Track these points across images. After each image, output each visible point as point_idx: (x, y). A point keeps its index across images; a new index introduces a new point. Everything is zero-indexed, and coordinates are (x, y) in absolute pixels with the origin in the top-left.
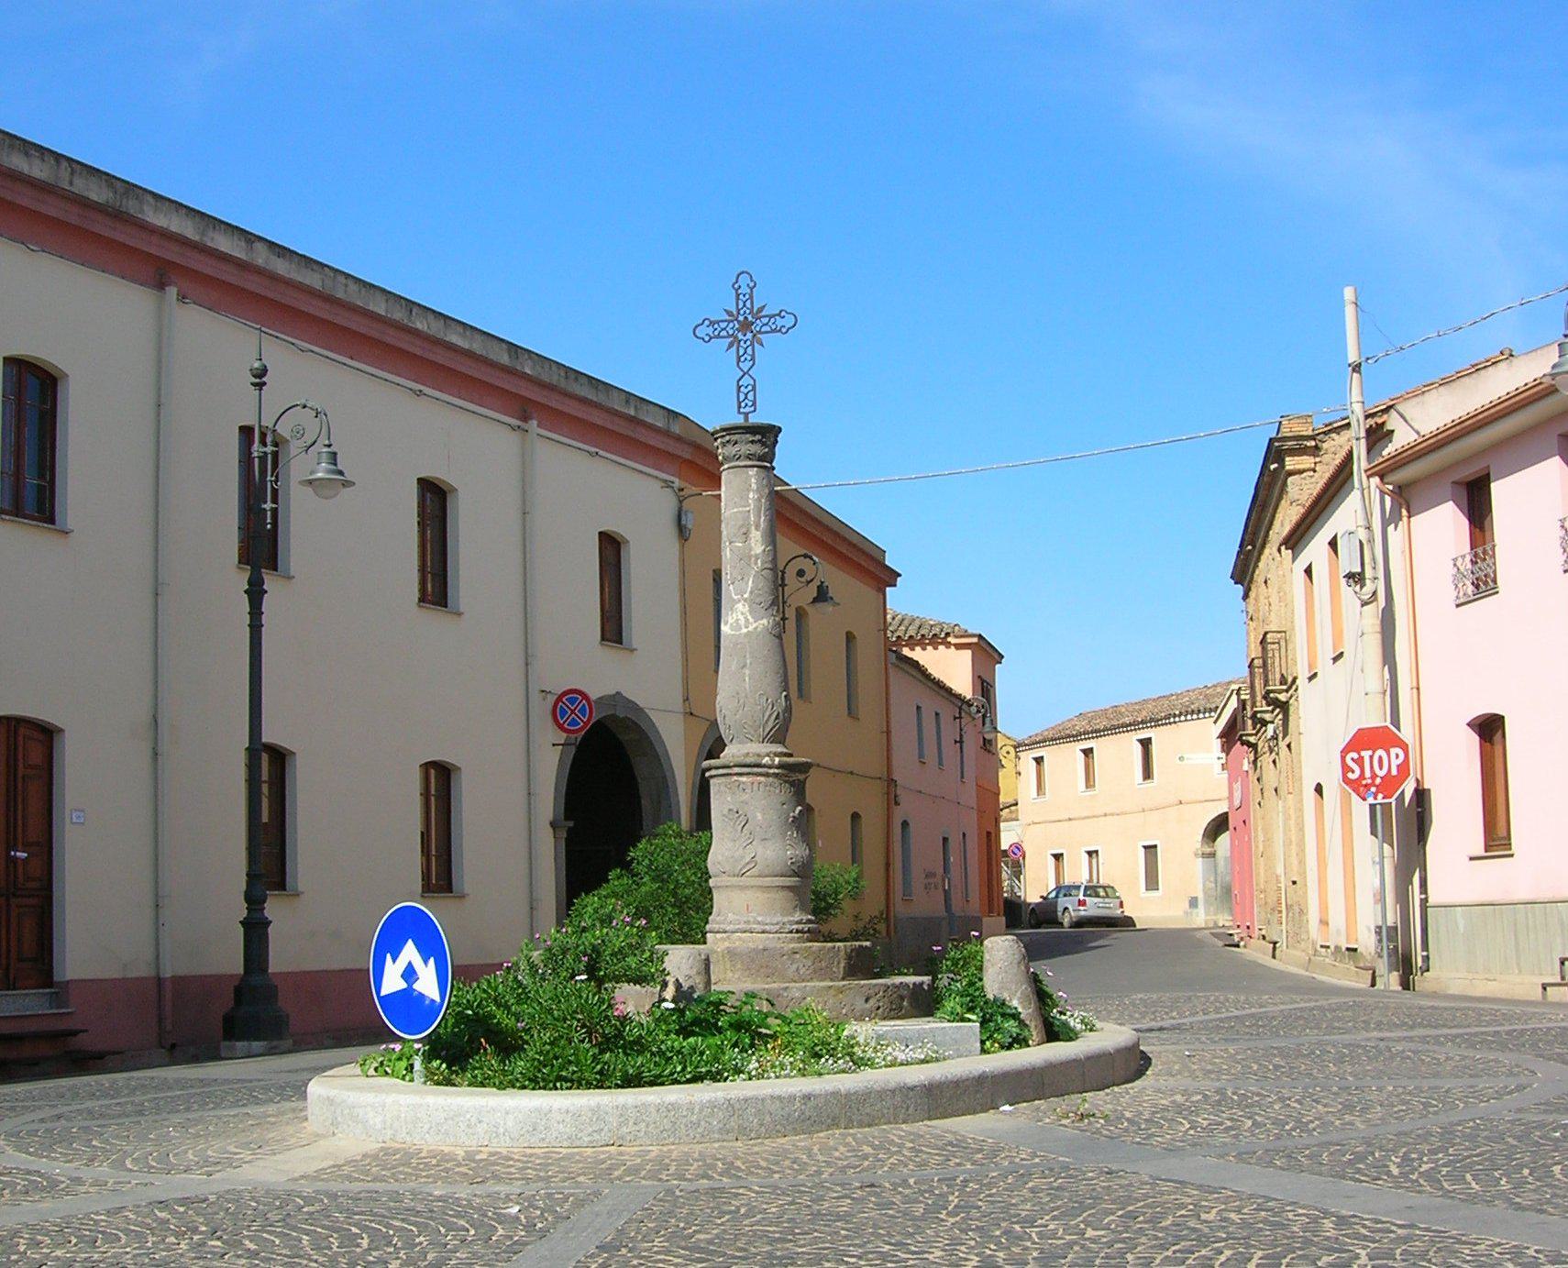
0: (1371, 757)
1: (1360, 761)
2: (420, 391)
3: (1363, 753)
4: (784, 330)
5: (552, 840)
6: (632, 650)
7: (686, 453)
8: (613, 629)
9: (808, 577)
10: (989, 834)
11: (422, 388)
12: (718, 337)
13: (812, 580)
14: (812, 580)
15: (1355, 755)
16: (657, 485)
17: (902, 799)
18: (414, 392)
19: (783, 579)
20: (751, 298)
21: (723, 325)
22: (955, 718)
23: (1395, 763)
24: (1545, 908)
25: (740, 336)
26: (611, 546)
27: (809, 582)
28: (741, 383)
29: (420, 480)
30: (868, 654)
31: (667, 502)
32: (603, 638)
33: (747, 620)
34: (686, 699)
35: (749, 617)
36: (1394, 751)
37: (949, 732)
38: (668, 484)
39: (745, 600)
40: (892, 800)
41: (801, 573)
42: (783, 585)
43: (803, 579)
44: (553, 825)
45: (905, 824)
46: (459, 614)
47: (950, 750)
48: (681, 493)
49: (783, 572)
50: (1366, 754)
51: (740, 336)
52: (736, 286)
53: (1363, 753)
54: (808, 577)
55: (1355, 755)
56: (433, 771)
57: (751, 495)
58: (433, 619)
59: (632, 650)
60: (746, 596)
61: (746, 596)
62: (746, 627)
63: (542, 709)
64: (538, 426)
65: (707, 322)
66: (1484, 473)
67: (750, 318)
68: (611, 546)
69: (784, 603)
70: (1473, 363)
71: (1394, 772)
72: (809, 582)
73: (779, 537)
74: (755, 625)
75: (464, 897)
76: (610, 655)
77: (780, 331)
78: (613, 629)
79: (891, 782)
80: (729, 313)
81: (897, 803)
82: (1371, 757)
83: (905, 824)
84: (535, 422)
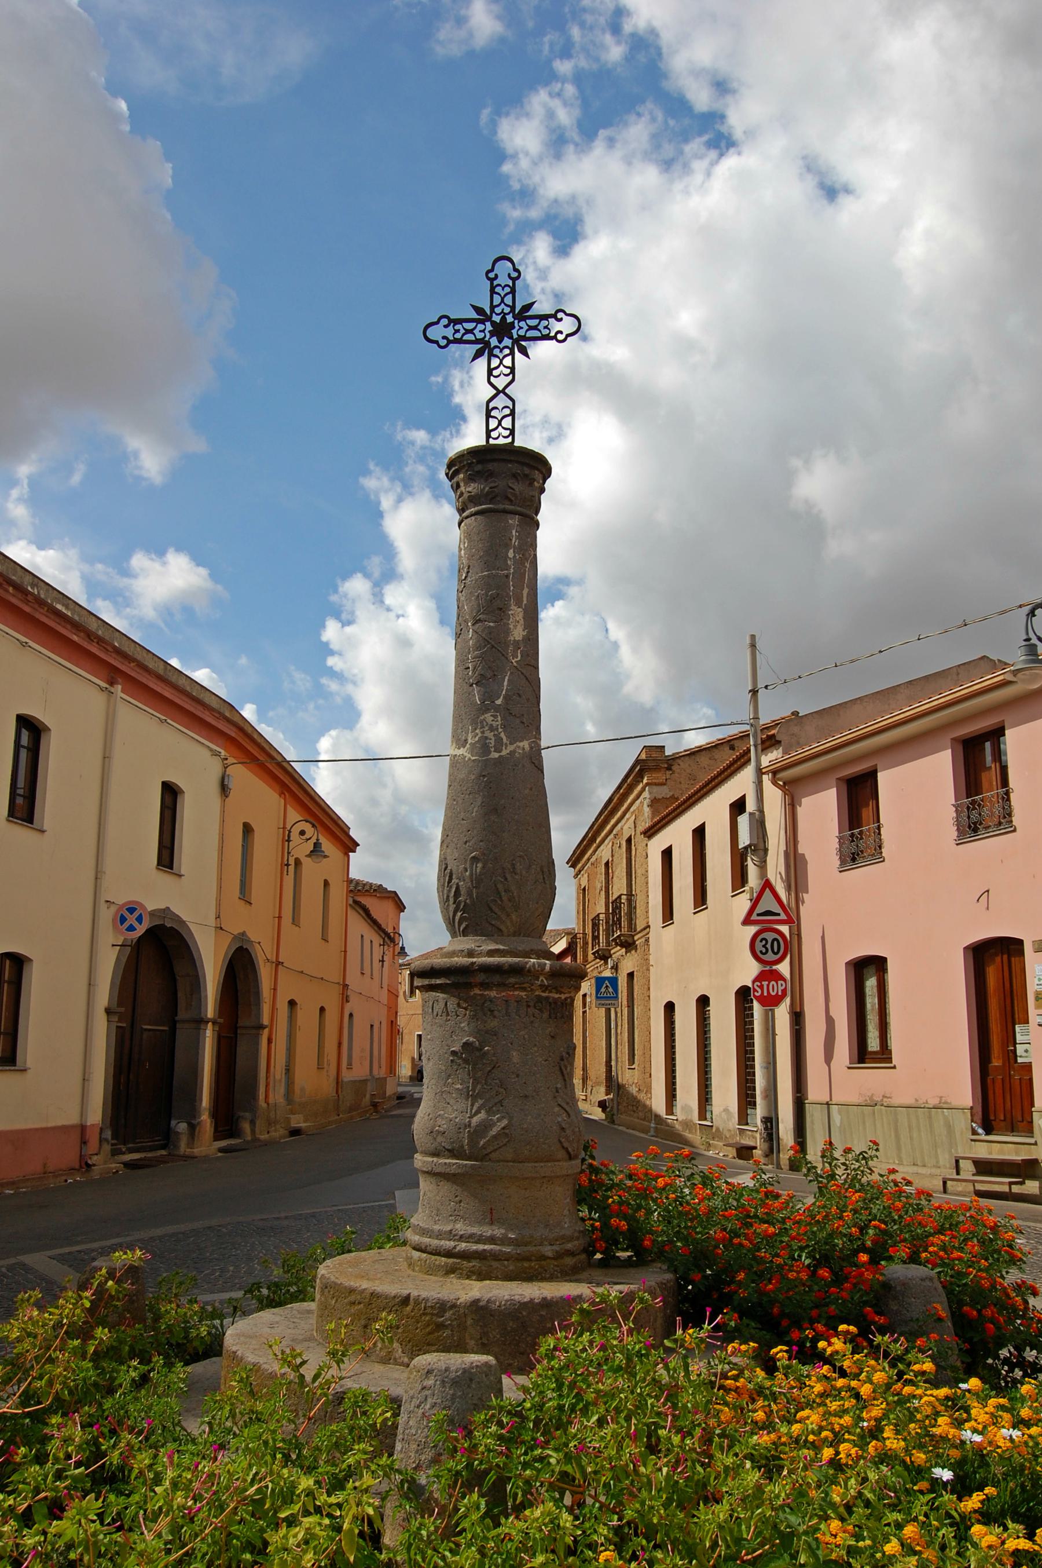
0: (768, 986)
1: (761, 986)
2: (26, 643)
3: (763, 983)
4: (560, 337)
5: (106, 1023)
6: (180, 876)
7: (232, 732)
8: (167, 858)
9: (307, 836)
10: (392, 1022)
11: (28, 641)
12: (460, 341)
13: (310, 839)
14: (310, 839)
15: (759, 984)
16: (208, 753)
17: (351, 999)
18: (21, 643)
19: (289, 836)
20: (513, 292)
21: (469, 326)
22: (380, 945)
23: (780, 988)
24: (930, 1113)
25: (494, 342)
26: (171, 793)
27: (308, 840)
28: (492, 405)
29: (18, 716)
30: (338, 896)
31: (215, 768)
32: (158, 864)
33: (498, 740)
34: (218, 917)
35: (502, 735)
36: (780, 982)
37: (378, 952)
38: (216, 754)
39: (497, 709)
40: (346, 999)
41: (302, 833)
42: (289, 841)
43: (304, 837)
44: (108, 1011)
45: (351, 1015)
46: (42, 832)
47: (377, 965)
48: (225, 762)
49: (290, 832)
50: (765, 983)
51: (494, 342)
52: (443, 343)
53: (763, 983)
54: (307, 836)
55: (759, 984)
56: (8, 962)
57: (511, 554)
58: (20, 833)
59: (180, 876)
60: (499, 702)
61: (499, 702)
62: (498, 750)
63: (107, 915)
64: (122, 692)
65: (445, 321)
66: (874, 769)
67: (510, 319)
68: (171, 793)
69: (289, 853)
70: (783, 716)
71: (780, 993)
72: (308, 840)
73: (289, 808)
74: (511, 748)
75: (25, 1070)
76: (164, 879)
77: (555, 338)
78: (167, 858)
79: (345, 986)
80: (479, 310)
81: (348, 1001)
82: (768, 986)
83: (351, 1015)
84: (120, 687)
